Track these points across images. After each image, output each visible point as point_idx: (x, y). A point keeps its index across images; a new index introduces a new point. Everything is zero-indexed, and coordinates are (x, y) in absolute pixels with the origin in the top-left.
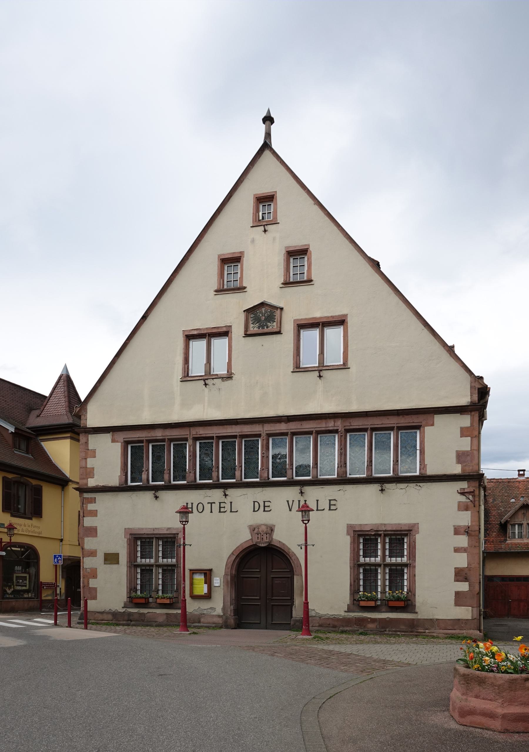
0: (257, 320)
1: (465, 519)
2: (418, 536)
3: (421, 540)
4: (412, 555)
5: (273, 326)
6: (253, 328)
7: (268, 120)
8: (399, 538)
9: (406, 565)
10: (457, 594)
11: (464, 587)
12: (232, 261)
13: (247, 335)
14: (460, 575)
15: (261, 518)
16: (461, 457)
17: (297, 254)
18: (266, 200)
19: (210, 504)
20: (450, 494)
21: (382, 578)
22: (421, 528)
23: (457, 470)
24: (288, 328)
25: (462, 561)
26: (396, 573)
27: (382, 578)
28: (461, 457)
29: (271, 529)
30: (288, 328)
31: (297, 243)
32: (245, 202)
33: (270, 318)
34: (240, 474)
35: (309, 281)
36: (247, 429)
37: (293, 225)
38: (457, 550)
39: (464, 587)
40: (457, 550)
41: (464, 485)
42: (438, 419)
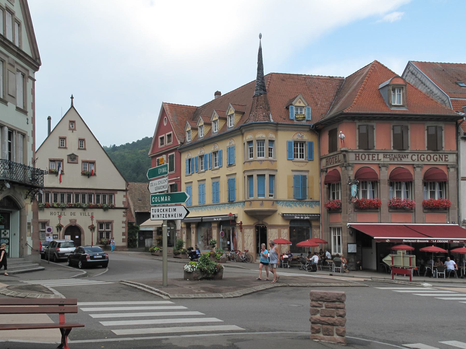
0: (71, 158)
1: (124, 219)
2: (114, 224)
3: (114, 225)
4: (112, 229)
5: (75, 161)
6: (70, 161)
7: (72, 98)
8: (109, 224)
9: (110, 231)
10: (123, 239)
11: (124, 237)
12: (63, 139)
13: (68, 163)
14: (124, 234)
15: (73, 217)
16: (124, 203)
17: (82, 141)
18: (72, 122)
19: (379, 159)
20: (121, 212)
21: (104, 235)
22: (115, 221)
23: (123, 206)
24: (80, 162)
25: (124, 230)
26: (108, 233)
27: (104, 235)
28: (124, 203)
29: (76, 221)
30: (80, 162)
31: (82, 137)
32: (66, 122)
33: (75, 158)
34: (255, 196)
35: (85, 149)
36: (69, 191)
37: (80, 133)
38: (123, 227)
39: (124, 237)
40: (123, 227)
41: (124, 210)
42: (118, 192)
